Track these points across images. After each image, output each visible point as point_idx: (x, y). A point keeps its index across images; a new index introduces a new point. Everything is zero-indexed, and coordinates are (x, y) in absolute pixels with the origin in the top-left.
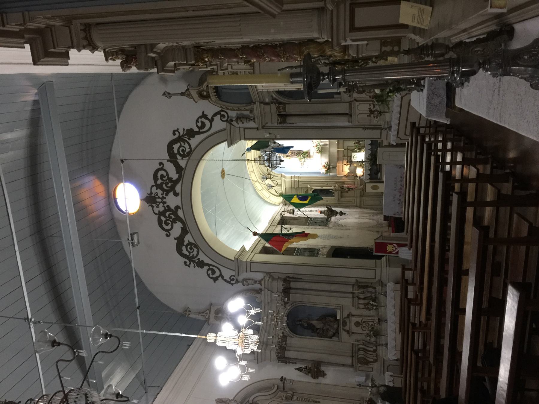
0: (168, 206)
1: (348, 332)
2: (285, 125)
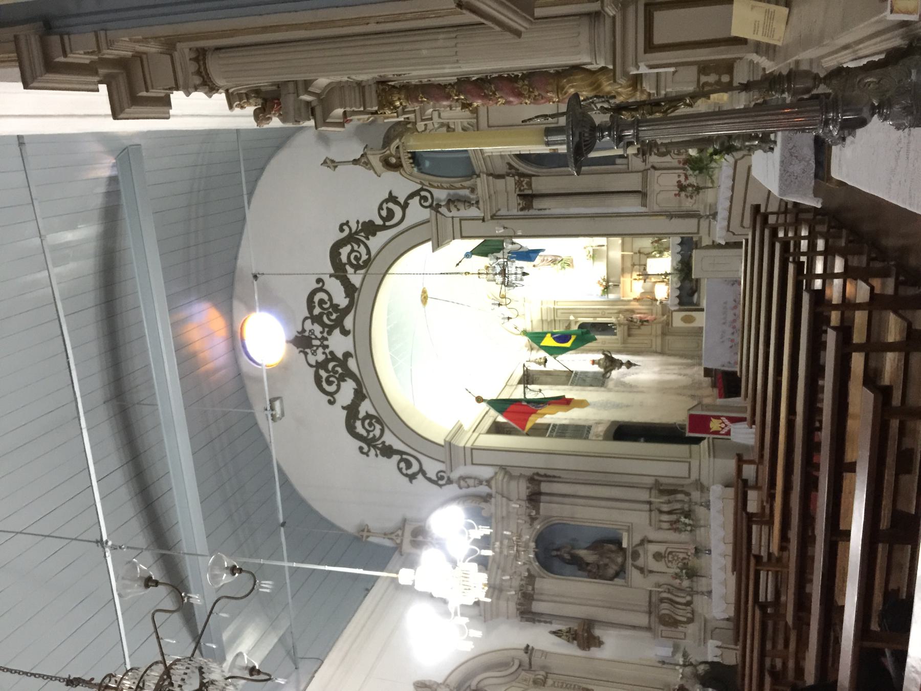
0: (332, 353)
1: (642, 570)
2: (532, 212)
